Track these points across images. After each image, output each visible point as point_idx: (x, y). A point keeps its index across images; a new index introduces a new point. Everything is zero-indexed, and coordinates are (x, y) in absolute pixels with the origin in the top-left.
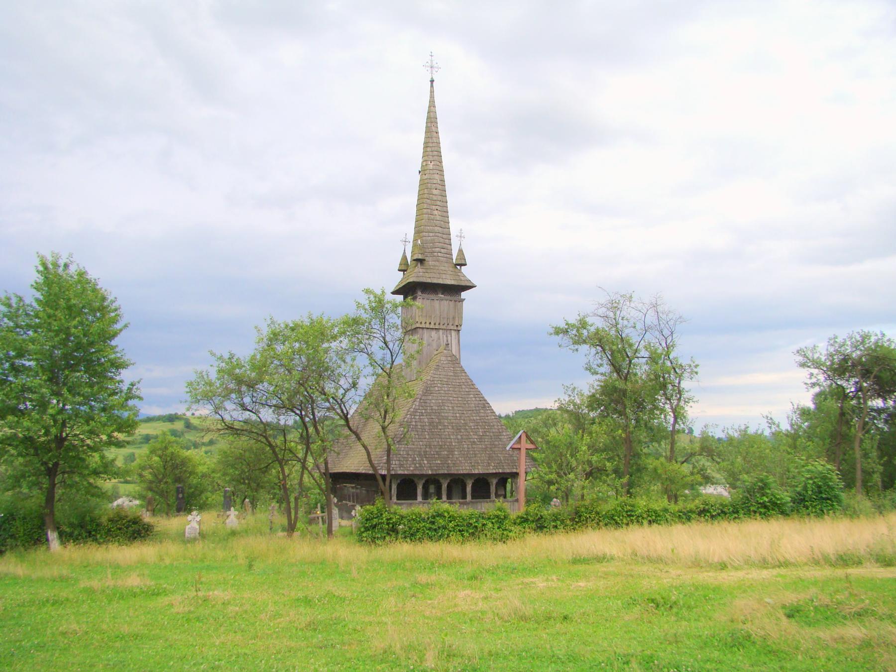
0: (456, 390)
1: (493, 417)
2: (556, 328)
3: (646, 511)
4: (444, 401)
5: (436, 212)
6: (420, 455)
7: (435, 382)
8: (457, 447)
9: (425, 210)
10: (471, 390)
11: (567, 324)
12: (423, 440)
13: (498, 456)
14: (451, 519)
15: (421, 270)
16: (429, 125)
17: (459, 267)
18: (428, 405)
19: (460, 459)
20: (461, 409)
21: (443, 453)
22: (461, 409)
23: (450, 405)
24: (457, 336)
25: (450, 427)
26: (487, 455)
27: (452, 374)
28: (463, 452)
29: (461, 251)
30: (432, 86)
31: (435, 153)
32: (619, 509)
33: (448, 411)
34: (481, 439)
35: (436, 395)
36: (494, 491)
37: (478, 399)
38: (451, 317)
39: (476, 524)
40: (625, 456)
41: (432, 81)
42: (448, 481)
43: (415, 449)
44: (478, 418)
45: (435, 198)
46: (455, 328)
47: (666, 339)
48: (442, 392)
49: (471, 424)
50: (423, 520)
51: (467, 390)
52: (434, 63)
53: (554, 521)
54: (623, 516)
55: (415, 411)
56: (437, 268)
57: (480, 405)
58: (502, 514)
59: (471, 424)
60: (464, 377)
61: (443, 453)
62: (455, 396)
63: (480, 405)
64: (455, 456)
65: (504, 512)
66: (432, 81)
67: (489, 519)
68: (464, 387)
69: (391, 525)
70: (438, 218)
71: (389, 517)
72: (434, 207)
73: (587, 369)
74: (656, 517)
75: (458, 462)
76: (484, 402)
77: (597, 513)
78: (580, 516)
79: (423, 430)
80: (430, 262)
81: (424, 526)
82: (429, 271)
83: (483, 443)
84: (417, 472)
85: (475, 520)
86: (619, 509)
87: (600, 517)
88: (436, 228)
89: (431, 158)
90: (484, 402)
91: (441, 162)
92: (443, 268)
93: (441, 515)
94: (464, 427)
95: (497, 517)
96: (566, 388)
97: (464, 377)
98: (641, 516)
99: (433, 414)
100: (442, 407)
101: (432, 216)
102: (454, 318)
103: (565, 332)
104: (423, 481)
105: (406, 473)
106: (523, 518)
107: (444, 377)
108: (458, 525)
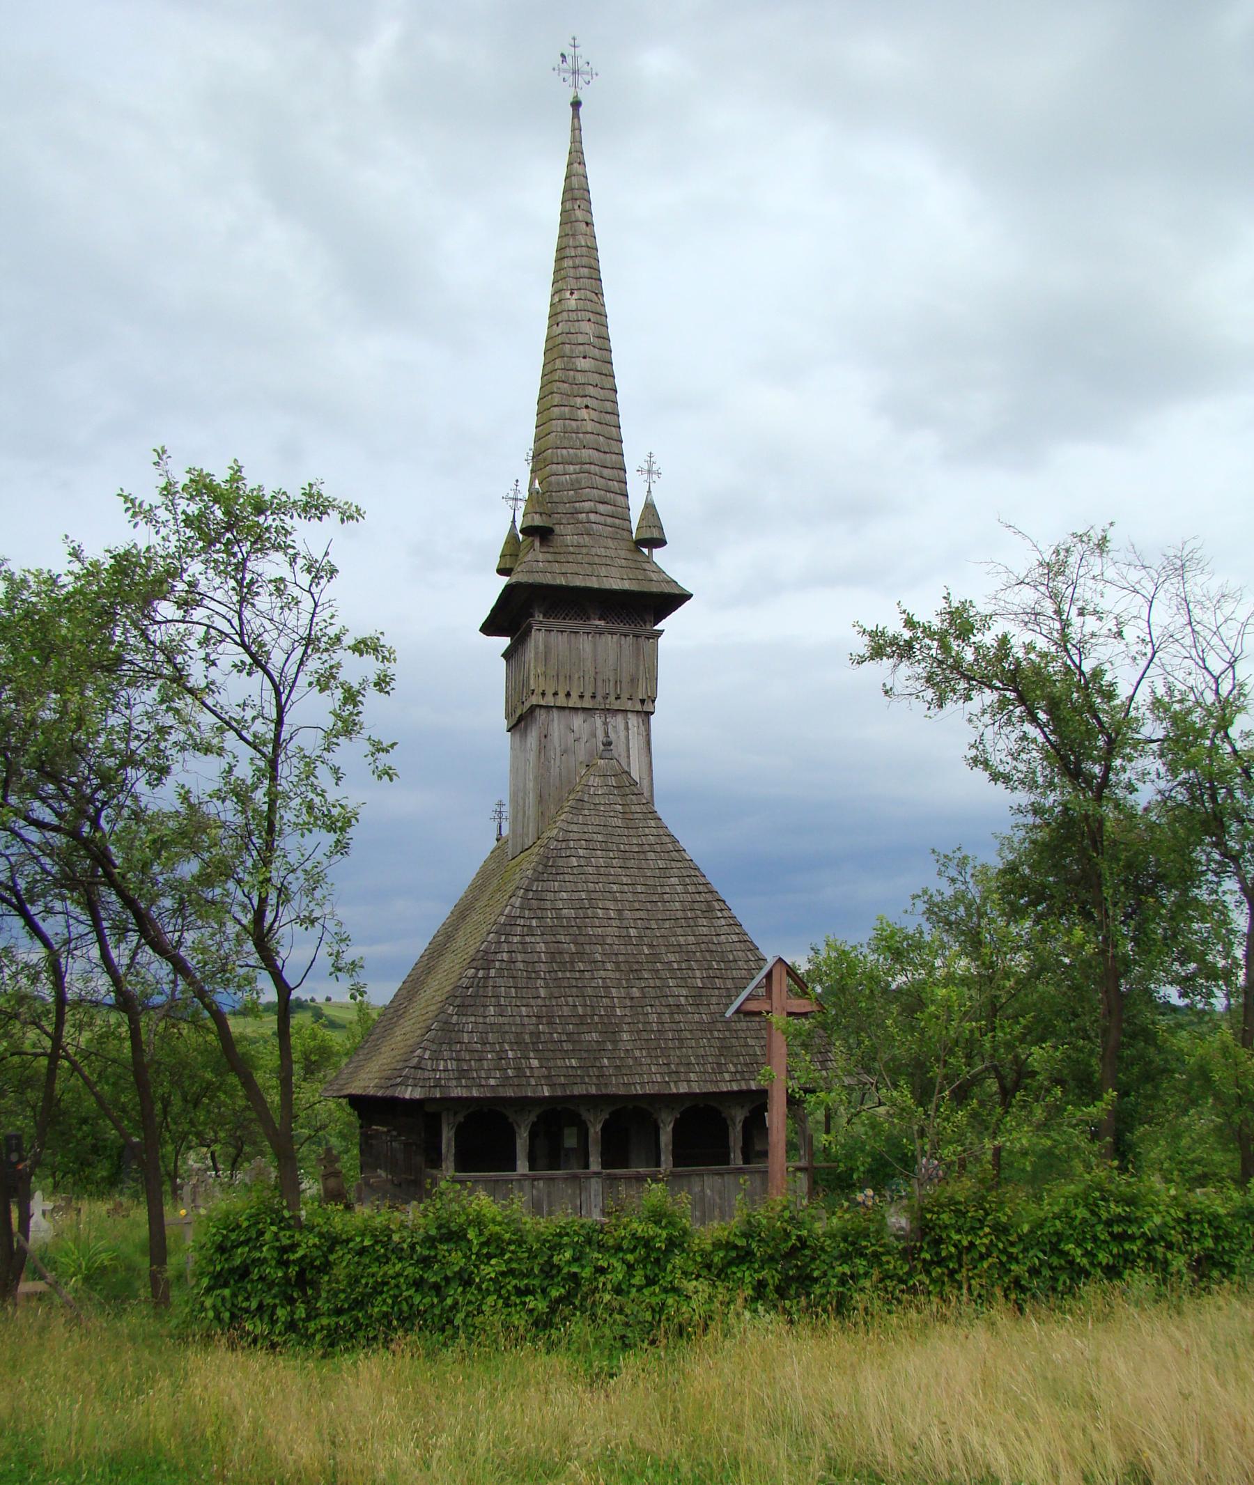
0: (631, 863)
1: (735, 938)
2: (873, 635)
3: (1178, 1221)
4: (593, 896)
5: (583, 413)
6: (518, 1043)
7: (572, 844)
8: (628, 1020)
9: (556, 409)
10: (674, 864)
11: (910, 623)
12: (532, 1002)
13: (747, 1045)
14: (492, 1249)
15: (541, 557)
16: (568, 205)
17: (645, 551)
18: (548, 905)
19: (637, 1053)
20: (642, 914)
21: (588, 1037)
22: (642, 914)
23: (611, 905)
24: (642, 728)
25: (609, 966)
26: (717, 1043)
27: (619, 823)
28: (645, 1035)
29: (650, 508)
30: (576, 116)
31: (584, 271)
32: (1081, 1213)
33: (605, 922)
34: (698, 998)
35: (571, 878)
36: (740, 1144)
37: (691, 888)
38: (626, 679)
39: (575, 1269)
40: (1105, 1031)
41: (576, 105)
42: (606, 1115)
43: (507, 1028)
44: (691, 939)
45: (580, 378)
46: (638, 707)
47: (1216, 679)
48: (590, 870)
49: (671, 957)
50: (398, 1250)
51: (661, 864)
52: (581, 62)
53: (845, 1257)
54: (1095, 1239)
55: (511, 921)
56: (584, 551)
57: (696, 906)
58: (661, 1235)
59: (671, 957)
60: (655, 831)
61: (588, 1037)
62: (625, 880)
63: (696, 906)
64: (621, 1045)
65: (671, 1224)
66: (576, 105)
67: (619, 1248)
68: (651, 855)
69: (293, 1271)
70: (590, 426)
71: (286, 1242)
72: (579, 400)
73: (975, 761)
74: (1217, 1239)
75: (631, 1062)
76: (709, 897)
77: (1001, 1230)
78: (938, 1242)
79: (532, 974)
80: (567, 535)
81: (398, 1275)
82: (559, 558)
83: (703, 1009)
84: (510, 1093)
85: (568, 1255)
86: (1081, 1213)
87: (1012, 1244)
88: (585, 453)
89: (572, 283)
90: (709, 897)
91: (599, 293)
92: (602, 551)
93: (454, 1236)
94: (650, 966)
95: (647, 1243)
96: (942, 860)
97: (655, 831)
98: (1162, 1237)
99: (561, 930)
100: (589, 911)
101: (574, 424)
102: (634, 681)
103: (905, 650)
104: (533, 1118)
105: (475, 1093)
106: (736, 1247)
107: (596, 829)
108: (511, 1272)
